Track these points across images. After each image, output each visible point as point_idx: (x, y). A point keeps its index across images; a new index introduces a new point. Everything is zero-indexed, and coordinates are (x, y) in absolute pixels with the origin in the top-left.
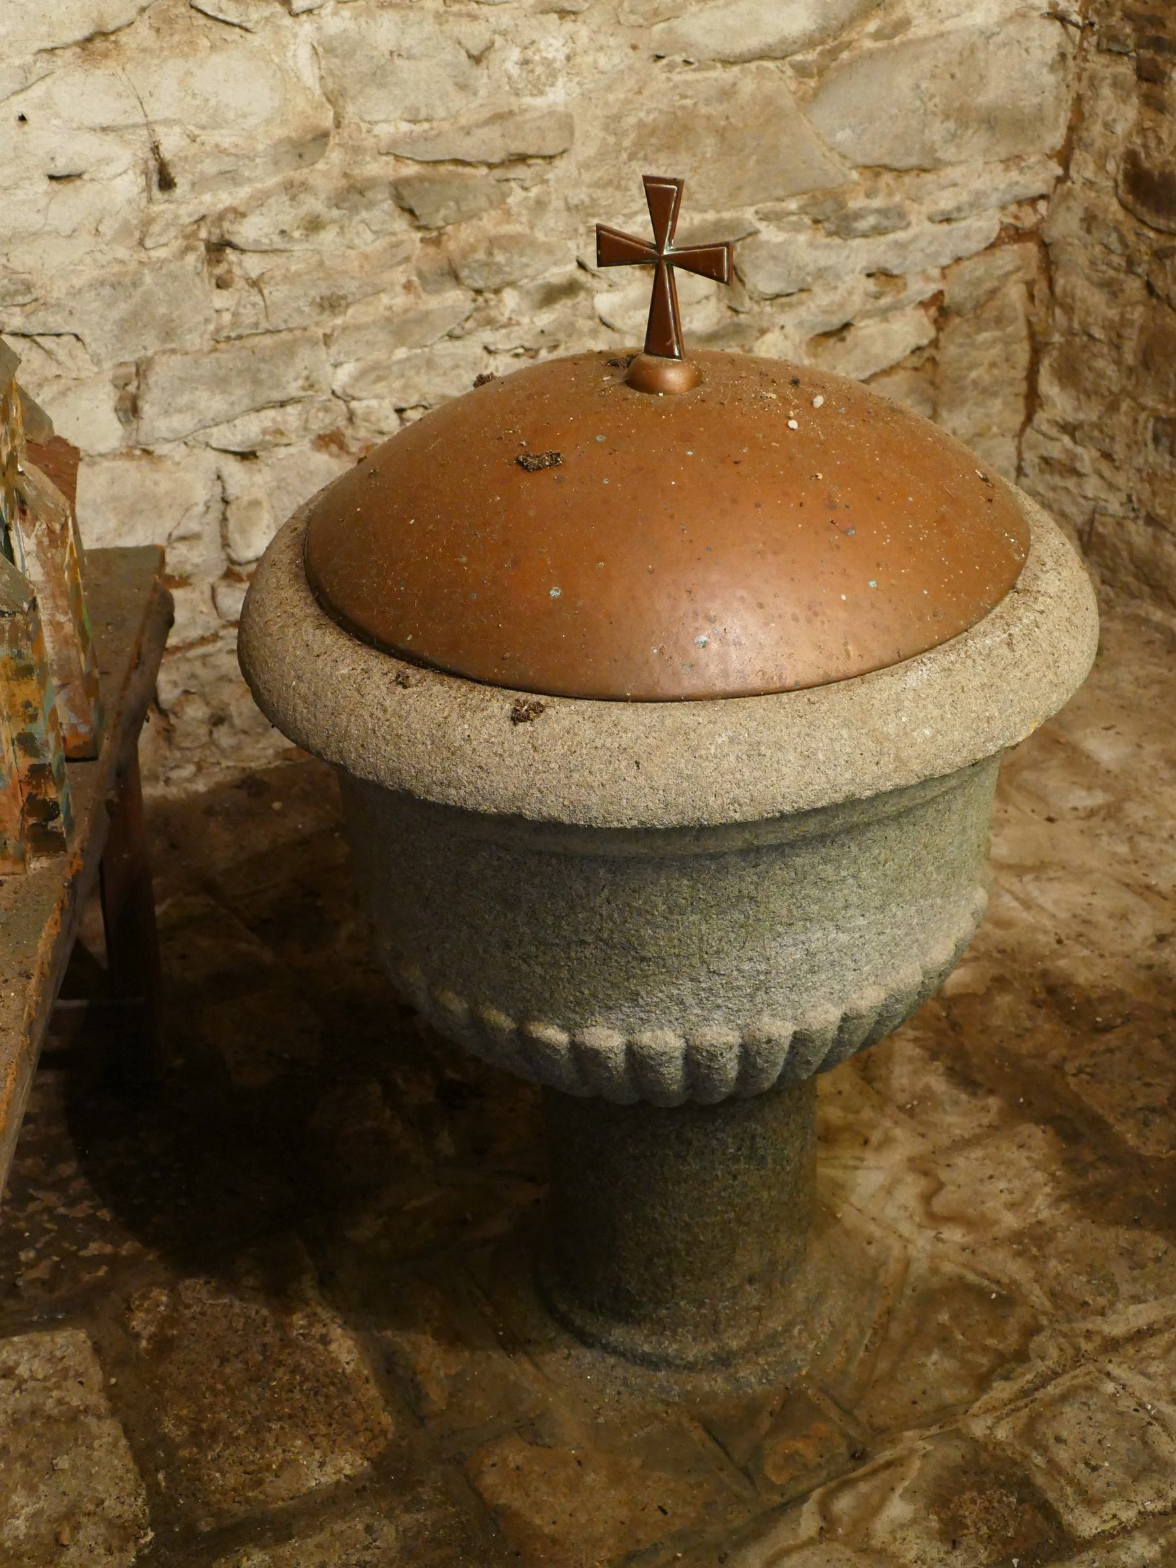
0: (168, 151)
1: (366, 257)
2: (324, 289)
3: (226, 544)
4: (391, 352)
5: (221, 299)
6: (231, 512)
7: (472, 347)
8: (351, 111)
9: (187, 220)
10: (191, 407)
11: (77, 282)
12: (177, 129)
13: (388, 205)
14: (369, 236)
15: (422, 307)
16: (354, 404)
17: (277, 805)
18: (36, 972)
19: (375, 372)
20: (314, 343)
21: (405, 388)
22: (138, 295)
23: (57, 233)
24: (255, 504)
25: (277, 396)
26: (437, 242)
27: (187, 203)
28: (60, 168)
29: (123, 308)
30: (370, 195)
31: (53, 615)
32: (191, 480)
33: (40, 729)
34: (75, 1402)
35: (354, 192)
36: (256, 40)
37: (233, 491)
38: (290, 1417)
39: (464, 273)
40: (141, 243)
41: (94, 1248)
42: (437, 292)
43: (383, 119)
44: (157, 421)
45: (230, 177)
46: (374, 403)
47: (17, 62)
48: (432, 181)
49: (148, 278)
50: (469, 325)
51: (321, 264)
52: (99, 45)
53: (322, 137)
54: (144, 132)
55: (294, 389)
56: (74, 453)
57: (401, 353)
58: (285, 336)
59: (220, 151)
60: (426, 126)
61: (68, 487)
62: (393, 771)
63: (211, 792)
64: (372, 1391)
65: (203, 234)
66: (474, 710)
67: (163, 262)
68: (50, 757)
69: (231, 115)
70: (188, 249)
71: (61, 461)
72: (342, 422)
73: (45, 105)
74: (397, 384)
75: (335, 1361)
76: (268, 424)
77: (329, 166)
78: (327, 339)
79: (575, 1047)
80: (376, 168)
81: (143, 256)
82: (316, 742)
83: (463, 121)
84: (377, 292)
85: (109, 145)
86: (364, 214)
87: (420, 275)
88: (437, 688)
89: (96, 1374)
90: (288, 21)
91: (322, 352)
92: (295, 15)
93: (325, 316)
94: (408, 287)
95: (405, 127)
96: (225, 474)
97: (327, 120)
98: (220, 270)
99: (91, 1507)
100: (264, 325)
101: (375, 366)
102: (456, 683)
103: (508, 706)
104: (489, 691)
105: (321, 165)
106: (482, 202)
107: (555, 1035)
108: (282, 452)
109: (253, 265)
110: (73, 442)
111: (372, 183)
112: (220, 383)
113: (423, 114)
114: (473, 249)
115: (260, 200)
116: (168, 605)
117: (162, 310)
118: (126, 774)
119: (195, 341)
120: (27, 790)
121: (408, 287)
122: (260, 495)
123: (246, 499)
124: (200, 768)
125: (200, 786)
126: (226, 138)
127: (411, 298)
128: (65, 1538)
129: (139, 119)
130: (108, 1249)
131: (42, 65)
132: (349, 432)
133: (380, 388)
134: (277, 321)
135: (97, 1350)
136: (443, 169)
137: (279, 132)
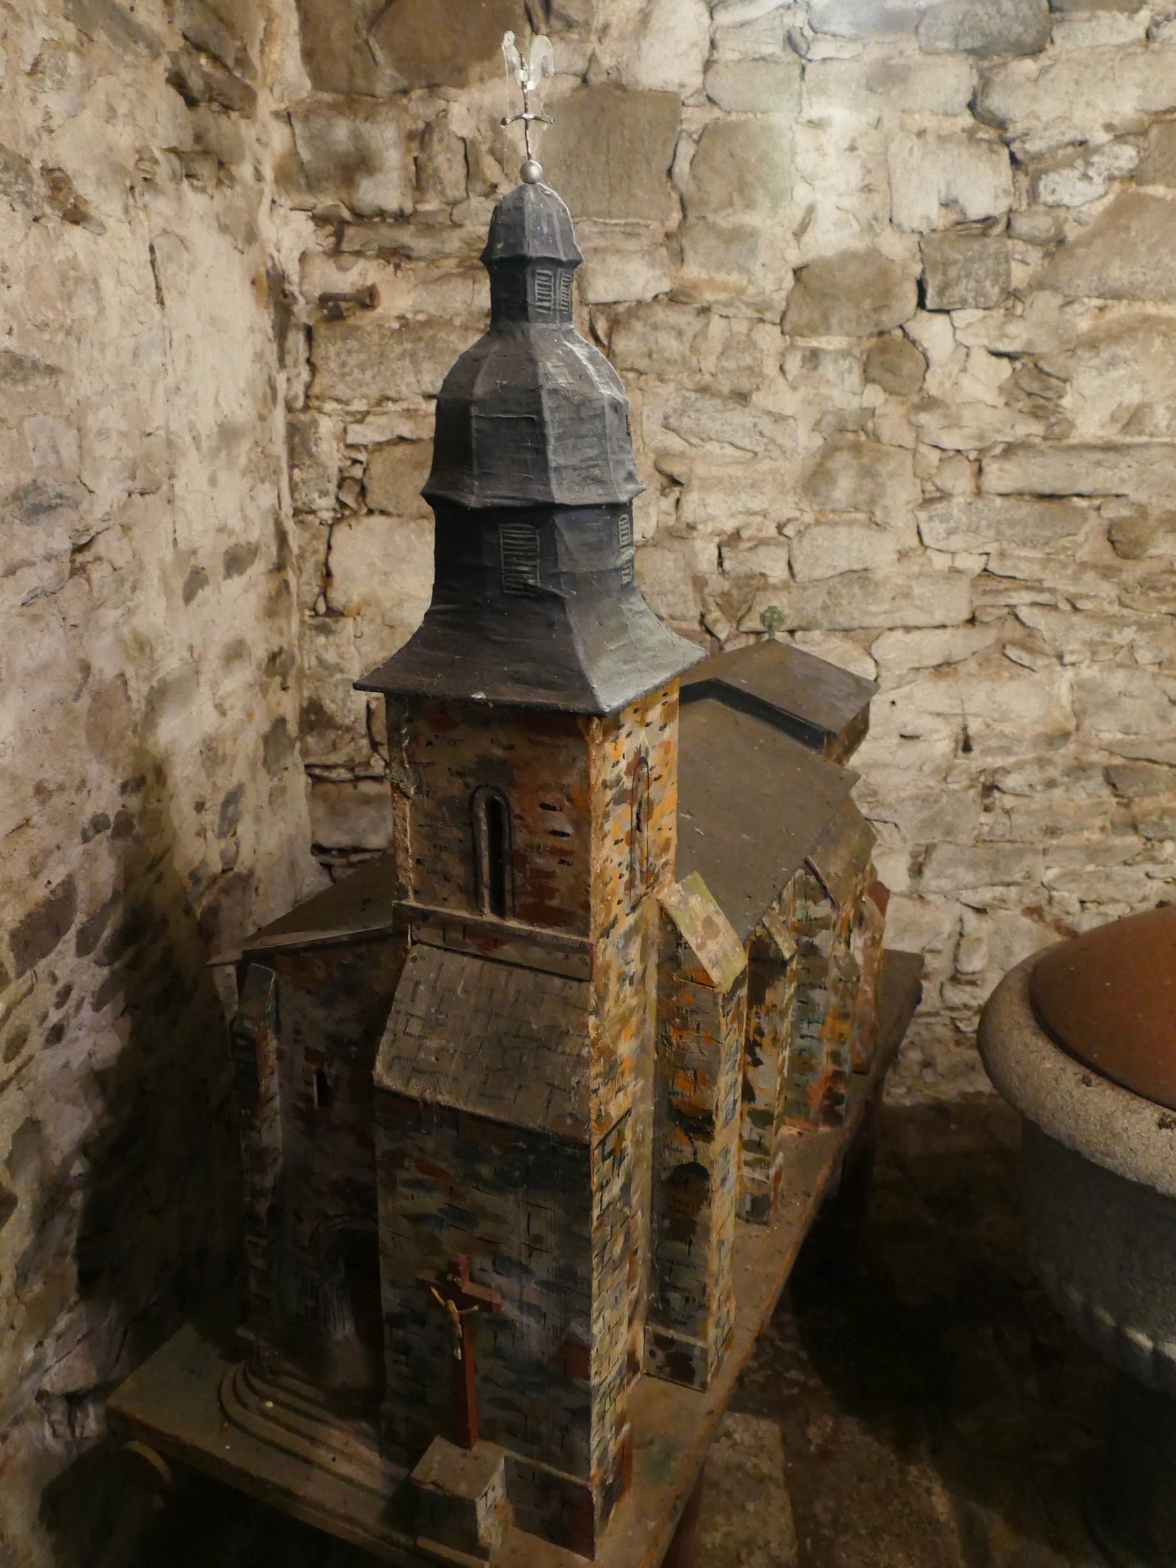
0: (971, 731)
1: (1079, 807)
2: (1049, 822)
3: (956, 959)
4: (1084, 865)
5: (985, 818)
6: (963, 942)
7: (1138, 872)
8: (1087, 723)
9: (974, 770)
10: (953, 877)
11: (903, 795)
12: (980, 720)
13: (1100, 779)
14: (1084, 795)
15: (1110, 842)
16: (1054, 893)
17: (953, 1126)
18: (814, 1194)
19: (1071, 876)
20: (1035, 852)
21: (1088, 889)
22: (936, 808)
23: (898, 767)
24: (979, 940)
25: (1007, 879)
26: (1127, 806)
27: (977, 761)
28: (908, 731)
29: (926, 814)
30: (1090, 772)
31: (126, 728)
32: (942, 919)
33: (845, 1051)
34: (765, 1470)
35: (1079, 769)
36: (1037, 677)
37: (968, 929)
38: (898, 1536)
39: (1141, 827)
40: (945, 779)
41: (793, 1374)
42: (1122, 835)
43: (1107, 730)
44: (931, 880)
45: (1006, 750)
46: (1066, 894)
47: (897, 672)
48: (1131, 769)
49: (944, 800)
50: (1139, 858)
51: (1050, 807)
52: (945, 669)
53: (1065, 735)
54: (960, 719)
55: (1018, 877)
56: (888, 892)
57: (1090, 868)
58: (1020, 846)
59: (1002, 735)
60: (1133, 737)
61: (883, 910)
62: (1070, 1136)
63: (912, 1107)
64: (955, 1540)
65: (982, 779)
66: (1133, 1112)
67: (955, 792)
68: (847, 1069)
69: (1013, 716)
70: (971, 787)
71: (881, 894)
72: (1044, 903)
73: (909, 697)
74: (1084, 886)
75: (933, 1508)
76: (997, 894)
77: (1065, 753)
78: (1045, 852)
79: (1157, 1355)
80: (1096, 757)
81: (944, 786)
82: (1022, 1105)
83: (1158, 737)
84: (1082, 829)
85: (938, 723)
86: (1083, 782)
87: (1112, 823)
88: (1109, 1092)
89: (780, 1456)
90: (1059, 668)
91: (1040, 859)
92: (1063, 665)
93: (1046, 839)
94: (1103, 829)
95: (1120, 736)
96: (965, 918)
97: (1071, 726)
98: (988, 801)
99: (761, 1543)
100: (1008, 837)
101: (1074, 873)
102: (1124, 1092)
103: (1157, 1116)
104: (1145, 1103)
105: (1062, 751)
106: (1162, 786)
107: (1144, 1341)
108: (1002, 913)
109: (1009, 801)
110: (887, 885)
111: (1092, 765)
112: (973, 865)
113: (1134, 729)
114: (1150, 813)
115: (1020, 766)
116: (919, 988)
117: (948, 818)
118: (878, 1087)
119: (964, 839)
120: (829, 1084)
121: (1103, 829)
122: (982, 934)
123: (975, 936)
124: (909, 1090)
125: (907, 1102)
126: (1008, 729)
127: (1104, 837)
128: (743, 1556)
129: (959, 711)
130: (802, 1378)
131: (911, 676)
132: (1047, 908)
133: (1073, 885)
134: (1016, 836)
135: (784, 1440)
136: (1139, 764)
137: (1040, 729)
